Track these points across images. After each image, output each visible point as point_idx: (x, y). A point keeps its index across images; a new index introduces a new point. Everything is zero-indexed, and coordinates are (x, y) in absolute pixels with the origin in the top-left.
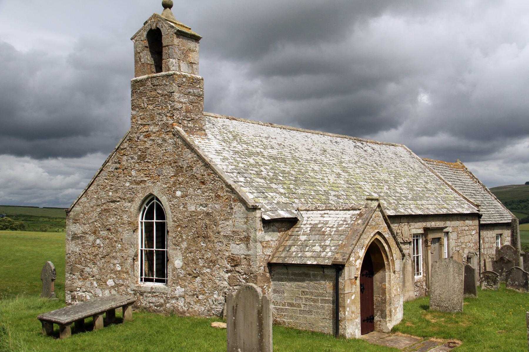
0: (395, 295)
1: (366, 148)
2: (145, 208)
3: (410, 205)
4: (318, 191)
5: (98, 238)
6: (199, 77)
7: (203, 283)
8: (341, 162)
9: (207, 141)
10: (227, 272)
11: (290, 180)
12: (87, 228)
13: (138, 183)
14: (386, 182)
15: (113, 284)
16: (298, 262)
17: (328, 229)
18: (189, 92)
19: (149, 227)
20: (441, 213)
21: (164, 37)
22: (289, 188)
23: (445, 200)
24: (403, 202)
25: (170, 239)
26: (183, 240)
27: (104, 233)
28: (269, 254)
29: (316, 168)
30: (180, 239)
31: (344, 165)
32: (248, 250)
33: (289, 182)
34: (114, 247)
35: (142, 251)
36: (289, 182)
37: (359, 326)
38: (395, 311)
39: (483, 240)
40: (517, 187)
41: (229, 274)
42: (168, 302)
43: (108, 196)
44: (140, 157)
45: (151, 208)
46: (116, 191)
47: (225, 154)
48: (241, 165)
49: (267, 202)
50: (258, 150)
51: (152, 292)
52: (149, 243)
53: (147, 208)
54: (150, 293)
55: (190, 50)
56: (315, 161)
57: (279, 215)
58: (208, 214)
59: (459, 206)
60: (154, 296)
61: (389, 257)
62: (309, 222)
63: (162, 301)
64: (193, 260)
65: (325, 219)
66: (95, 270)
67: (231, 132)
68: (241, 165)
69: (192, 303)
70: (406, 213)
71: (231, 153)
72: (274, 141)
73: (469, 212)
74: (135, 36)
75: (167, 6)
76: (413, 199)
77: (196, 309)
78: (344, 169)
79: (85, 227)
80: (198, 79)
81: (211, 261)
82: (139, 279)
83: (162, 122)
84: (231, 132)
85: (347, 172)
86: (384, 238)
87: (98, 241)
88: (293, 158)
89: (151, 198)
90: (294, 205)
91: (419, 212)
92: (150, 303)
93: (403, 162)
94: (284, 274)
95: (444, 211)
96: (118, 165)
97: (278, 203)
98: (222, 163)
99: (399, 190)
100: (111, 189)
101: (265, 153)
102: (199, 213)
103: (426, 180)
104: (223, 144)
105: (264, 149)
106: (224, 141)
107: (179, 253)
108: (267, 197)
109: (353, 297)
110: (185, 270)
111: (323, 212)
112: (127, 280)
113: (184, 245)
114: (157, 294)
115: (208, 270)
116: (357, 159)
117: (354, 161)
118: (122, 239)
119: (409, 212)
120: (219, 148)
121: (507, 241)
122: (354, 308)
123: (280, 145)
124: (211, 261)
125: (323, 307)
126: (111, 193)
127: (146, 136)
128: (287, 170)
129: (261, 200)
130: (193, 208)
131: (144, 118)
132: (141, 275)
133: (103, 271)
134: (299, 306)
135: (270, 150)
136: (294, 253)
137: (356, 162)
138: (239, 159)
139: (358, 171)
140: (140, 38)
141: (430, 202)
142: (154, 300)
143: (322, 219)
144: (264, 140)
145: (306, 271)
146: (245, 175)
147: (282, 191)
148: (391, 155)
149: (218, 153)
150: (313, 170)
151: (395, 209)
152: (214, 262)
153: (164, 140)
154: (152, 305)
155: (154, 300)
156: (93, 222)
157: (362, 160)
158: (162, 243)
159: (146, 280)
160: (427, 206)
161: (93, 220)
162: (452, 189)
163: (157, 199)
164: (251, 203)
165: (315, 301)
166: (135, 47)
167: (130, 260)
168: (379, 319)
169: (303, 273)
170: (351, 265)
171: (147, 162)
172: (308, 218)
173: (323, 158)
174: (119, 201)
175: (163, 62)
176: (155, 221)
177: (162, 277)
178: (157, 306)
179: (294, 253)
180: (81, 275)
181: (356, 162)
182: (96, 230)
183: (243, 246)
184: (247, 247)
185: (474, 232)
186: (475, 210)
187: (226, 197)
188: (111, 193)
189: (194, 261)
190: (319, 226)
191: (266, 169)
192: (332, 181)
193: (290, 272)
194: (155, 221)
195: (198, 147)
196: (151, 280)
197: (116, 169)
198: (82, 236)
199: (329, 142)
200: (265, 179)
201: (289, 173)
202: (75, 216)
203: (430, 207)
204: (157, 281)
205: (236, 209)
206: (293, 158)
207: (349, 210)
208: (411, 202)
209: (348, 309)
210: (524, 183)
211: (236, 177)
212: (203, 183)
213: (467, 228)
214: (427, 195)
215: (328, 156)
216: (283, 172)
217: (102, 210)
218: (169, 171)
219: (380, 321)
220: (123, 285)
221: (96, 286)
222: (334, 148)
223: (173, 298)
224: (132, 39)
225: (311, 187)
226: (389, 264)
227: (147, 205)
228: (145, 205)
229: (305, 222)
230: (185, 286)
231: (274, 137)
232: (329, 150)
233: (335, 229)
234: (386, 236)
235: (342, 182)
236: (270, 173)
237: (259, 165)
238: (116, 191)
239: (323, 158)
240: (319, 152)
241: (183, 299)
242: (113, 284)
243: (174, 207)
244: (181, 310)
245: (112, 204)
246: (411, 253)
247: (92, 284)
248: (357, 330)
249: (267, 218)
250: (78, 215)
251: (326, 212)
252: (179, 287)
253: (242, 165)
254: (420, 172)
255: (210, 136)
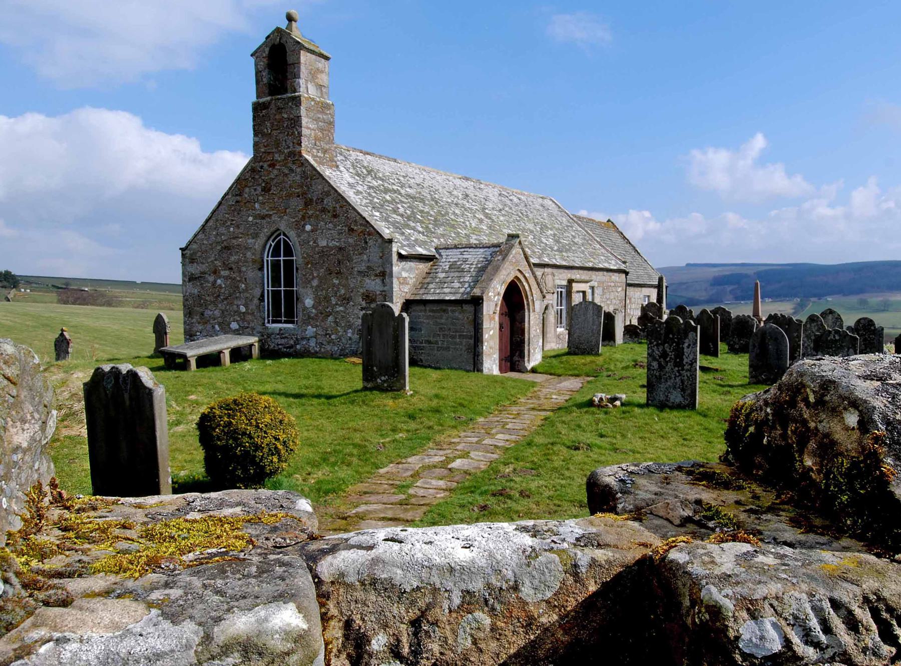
0: (534, 336)
1: (511, 198)
2: (271, 245)
3: (555, 255)
4: (459, 233)
5: (220, 278)
6: (330, 102)
7: (335, 322)
8: (484, 209)
9: (339, 173)
10: (362, 309)
11: (429, 220)
12: (203, 267)
13: (263, 218)
14: (532, 232)
15: (237, 327)
16: (436, 298)
17: (468, 266)
18: (319, 118)
19: (276, 266)
20: (587, 265)
21: (289, 53)
22: (427, 227)
23: (592, 254)
24: (547, 252)
25: (297, 277)
26: (314, 278)
27: (225, 273)
28: (406, 290)
29: (457, 211)
30: (311, 277)
31: (487, 211)
32: (384, 286)
33: (427, 222)
34: (238, 287)
35: (268, 291)
36: (427, 222)
37: (497, 362)
38: (534, 351)
39: (630, 299)
40: (715, 272)
41: (364, 312)
42: (298, 344)
43: (229, 232)
44: (264, 190)
45: (278, 245)
46: (238, 227)
47: (360, 188)
48: (376, 200)
49: (404, 237)
50: (395, 187)
51: (281, 332)
52: (276, 281)
53: (273, 244)
54: (278, 334)
55: (318, 70)
56: (456, 204)
57: (418, 251)
58: (340, 249)
59: (606, 261)
60: (284, 338)
61: (529, 297)
62: (448, 260)
63: (292, 342)
64: (325, 298)
65: (465, 256)
66: (217, 313)
67: (365, 167)
68: (376, 200)
69: (324, 343)
70: (551, 263)
71: (366, 187)
72: (412, 181)
73: (615, 268)
74: (256, 52)
75: (290, 18)
76: (558, 250)
77: (329, 349)
78: (487, 216)
79: (204, 266)
80: (328, 104)
81: (344, 299)
82: (266, 321)
83: (289, 150)
84: (365, 167)
85: (490, 218)
86: (525, 276)
87: (219, 281)
88: (433, 199)
89: (276, 232)
90: (433, 244)
91: (564, 263)
92: (278, 345)
93: (551, 215)
94: (421, 311)
95: (590, 265)
96: (239, 198)
97: (416, 240)
98: (355, 196)
99: (544, 240)
100: (231, 224)
101: (403, 192)
102: (331, 248)
103: (574, 234)
104: (356, 177)
105: (401, 187)
106: (359, 175)
107: (310, 291)
108: (404, 233)
109: (491, 333)
110: (316, 309)
111: (463, 250)
112: (253, 321)
113: (315, 283)
114: (287, 335)
115: (341, 308)
116: (501, 207)
117: (498, 209)
118: (245, 279)
119: (554, 262)
120: (351, 181)
121: (654, 299)
122: (492, 343)
123: (418, 185)
124: (344, 299)
125: (461, 343)
126: (232, 229)
127: (270, 166)
128: (426, 210)
129: (397, 235)
130: (323, 243)
131: (268, 145)
132: (268, 317)
133: (226, 313)
134: (437, 343)
135: (408, 190)
136: (432, 290)
137: (501, 210)
138: (374, 194)
139: (502, 218)
140: (262, 55)
141: (576, 255)
142: (283, 341)
143: (461, 256)
144: (402, 178)
145: (444, 307)
146: (381, 210)
147: (421, 229)
148: (538, 207)
149: (351, 186)
150: (454, 213)
151: (539, 258)
152: (348, 300)
153: (291, 170)
154: (280, 347)
155: (283, 341)
156: (212, 261)
157: (507, 209)
158: (289, 282)
159: (274, 322)
160: (573, 258)
161: (213, 259)
162: (601, 245)
163: (285, 235)
164: (387, 237)
165: (453, 337)
166: (256, 65)
167: (256, 301)
168: (517, 359)
169: (441, 309)
170: (489, 299)
171: (273, 194)
172: (447, 256)
173: (465, 202)
174: (241, 238)
175: (289, 82)
176: (282, 288)
177: (290, 317)
178: (287, 348)
179: (432, 290)
180: (201, 319)
181: (501, 210)
182: (216, 270)
183: (378, 281)
184: (383, 282)
185: (620, 289)
186: (623, 267)
187: (360, 230)
188: (232, 229)
189: (327, 299)
190: (458, 263)
191: (403, 207)
192: (473, 225)
193: (428, 309)
194: (282, 288)
195: (330, 178)
196: (280, 322)
197: (237, 202)
198: (201, 277)
199: (472, 188)
200: (402, 216)
201: (428, 213)
202: (191, 255)
203: (576, 259)
204: (286, 322)
205: (371, 243)
206: (433, 199)
207: (489, 247)
208: (556, 253)
209: (486, 344)
210: (684, 265)
211: (371, 211)
212: (335, 216)
213: (613, 284)
214: (573, 248)
215: (470, 201)
216: (422, 212)
217: (222, 248)
218: (296, 203)
219: (519, 361)
220: (248, 327)
221: (218, 329)
222: (477, 194)
223: (303, 339)
224: (252, 55)
225: (452, 229)
226: (528, 304)
227: (273, 242)
228: (270, 241)
229: (444, 260)
230: (317, 326)
231: (412, 176)
232: (472, 195)
233: (474, 266)
234: (527, 275)
235: (485, 228)
236: (407, 211)
237: (396, 202)
238: (238, 227)
239: (465, 202)
240: (461, 197)
241: (315, 339)
242: (237, 327)
243: (304, 243)
244: (313, 351)
245: (234, 241)
246: (555, 304)
247: (213, 327)
248: (494, 366)
249: (403, 253)
250: (195, 253)
251: (466, 250)
252: (310, 327)
253: (378, 201)
254: (567, 226)
255: (342, 169)
